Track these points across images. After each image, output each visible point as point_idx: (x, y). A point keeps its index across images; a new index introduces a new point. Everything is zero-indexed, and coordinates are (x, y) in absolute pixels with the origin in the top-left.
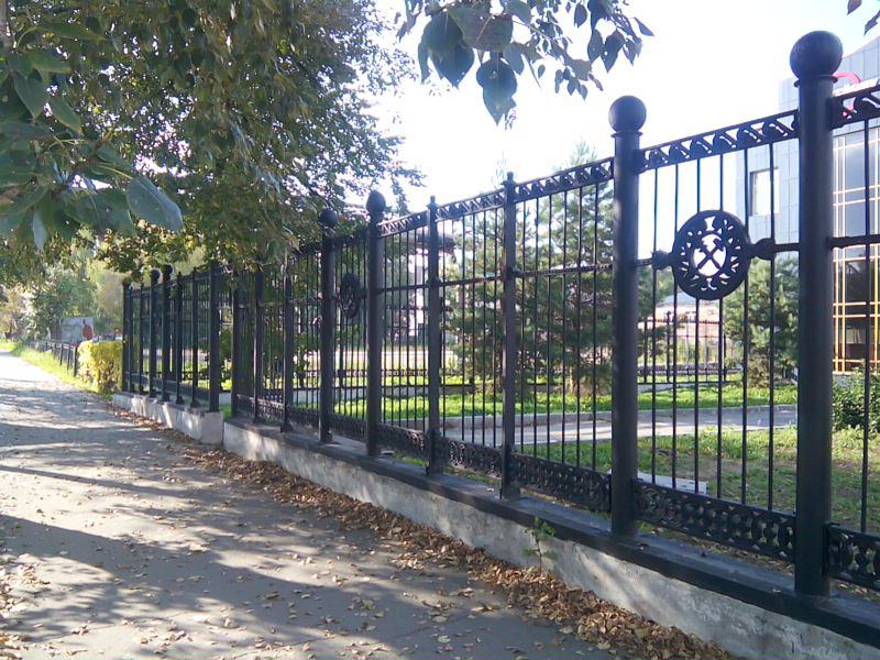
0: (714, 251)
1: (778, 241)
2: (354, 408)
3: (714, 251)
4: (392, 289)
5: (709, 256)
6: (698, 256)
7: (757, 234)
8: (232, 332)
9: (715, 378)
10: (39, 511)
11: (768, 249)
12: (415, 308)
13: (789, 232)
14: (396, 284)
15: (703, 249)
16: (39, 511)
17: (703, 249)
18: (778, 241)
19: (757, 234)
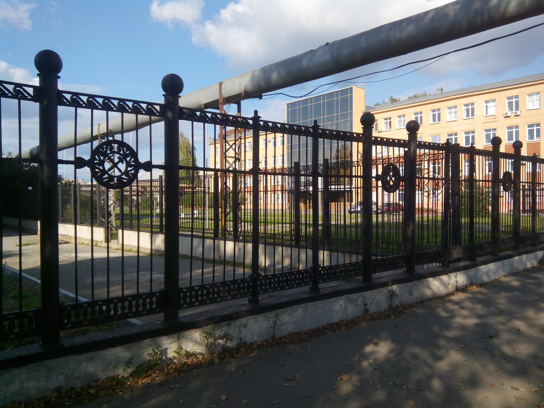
0: (118, 163)
1: (73, 166)
2: (380, 219)
3: (118, 163)
4: (482, 181)
5: (115, 165)
6: (107, 165)
7: (143, 158)
8: (440, 224)
9: (201, 234)
10: (283, 366)
11: (148, 166)
12: (263, 191)
13: (159, 158)
14: (484, 179)
15: (112, 161)
16: (283, 366)
17: (112, 161)
18: (73, 166)
19: (143, 158)
